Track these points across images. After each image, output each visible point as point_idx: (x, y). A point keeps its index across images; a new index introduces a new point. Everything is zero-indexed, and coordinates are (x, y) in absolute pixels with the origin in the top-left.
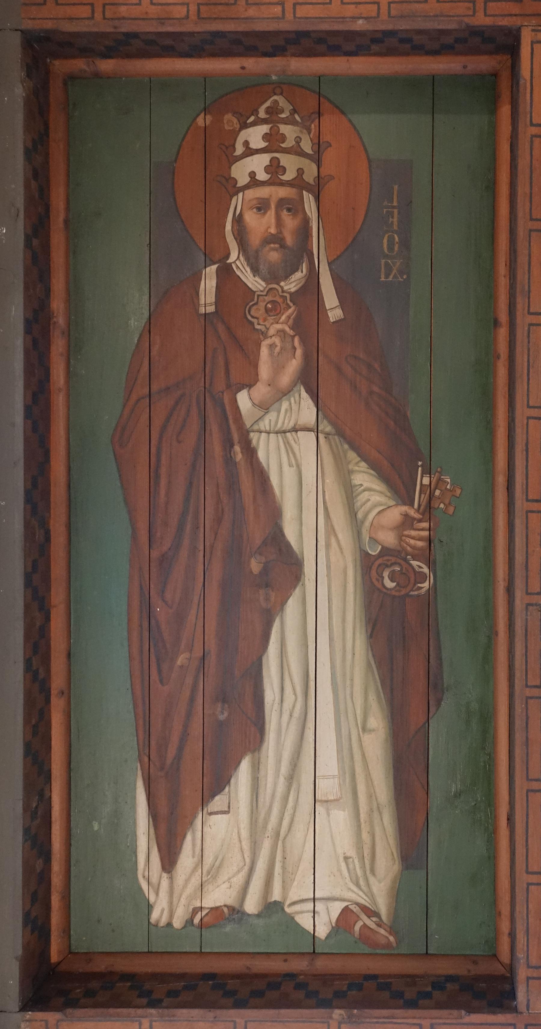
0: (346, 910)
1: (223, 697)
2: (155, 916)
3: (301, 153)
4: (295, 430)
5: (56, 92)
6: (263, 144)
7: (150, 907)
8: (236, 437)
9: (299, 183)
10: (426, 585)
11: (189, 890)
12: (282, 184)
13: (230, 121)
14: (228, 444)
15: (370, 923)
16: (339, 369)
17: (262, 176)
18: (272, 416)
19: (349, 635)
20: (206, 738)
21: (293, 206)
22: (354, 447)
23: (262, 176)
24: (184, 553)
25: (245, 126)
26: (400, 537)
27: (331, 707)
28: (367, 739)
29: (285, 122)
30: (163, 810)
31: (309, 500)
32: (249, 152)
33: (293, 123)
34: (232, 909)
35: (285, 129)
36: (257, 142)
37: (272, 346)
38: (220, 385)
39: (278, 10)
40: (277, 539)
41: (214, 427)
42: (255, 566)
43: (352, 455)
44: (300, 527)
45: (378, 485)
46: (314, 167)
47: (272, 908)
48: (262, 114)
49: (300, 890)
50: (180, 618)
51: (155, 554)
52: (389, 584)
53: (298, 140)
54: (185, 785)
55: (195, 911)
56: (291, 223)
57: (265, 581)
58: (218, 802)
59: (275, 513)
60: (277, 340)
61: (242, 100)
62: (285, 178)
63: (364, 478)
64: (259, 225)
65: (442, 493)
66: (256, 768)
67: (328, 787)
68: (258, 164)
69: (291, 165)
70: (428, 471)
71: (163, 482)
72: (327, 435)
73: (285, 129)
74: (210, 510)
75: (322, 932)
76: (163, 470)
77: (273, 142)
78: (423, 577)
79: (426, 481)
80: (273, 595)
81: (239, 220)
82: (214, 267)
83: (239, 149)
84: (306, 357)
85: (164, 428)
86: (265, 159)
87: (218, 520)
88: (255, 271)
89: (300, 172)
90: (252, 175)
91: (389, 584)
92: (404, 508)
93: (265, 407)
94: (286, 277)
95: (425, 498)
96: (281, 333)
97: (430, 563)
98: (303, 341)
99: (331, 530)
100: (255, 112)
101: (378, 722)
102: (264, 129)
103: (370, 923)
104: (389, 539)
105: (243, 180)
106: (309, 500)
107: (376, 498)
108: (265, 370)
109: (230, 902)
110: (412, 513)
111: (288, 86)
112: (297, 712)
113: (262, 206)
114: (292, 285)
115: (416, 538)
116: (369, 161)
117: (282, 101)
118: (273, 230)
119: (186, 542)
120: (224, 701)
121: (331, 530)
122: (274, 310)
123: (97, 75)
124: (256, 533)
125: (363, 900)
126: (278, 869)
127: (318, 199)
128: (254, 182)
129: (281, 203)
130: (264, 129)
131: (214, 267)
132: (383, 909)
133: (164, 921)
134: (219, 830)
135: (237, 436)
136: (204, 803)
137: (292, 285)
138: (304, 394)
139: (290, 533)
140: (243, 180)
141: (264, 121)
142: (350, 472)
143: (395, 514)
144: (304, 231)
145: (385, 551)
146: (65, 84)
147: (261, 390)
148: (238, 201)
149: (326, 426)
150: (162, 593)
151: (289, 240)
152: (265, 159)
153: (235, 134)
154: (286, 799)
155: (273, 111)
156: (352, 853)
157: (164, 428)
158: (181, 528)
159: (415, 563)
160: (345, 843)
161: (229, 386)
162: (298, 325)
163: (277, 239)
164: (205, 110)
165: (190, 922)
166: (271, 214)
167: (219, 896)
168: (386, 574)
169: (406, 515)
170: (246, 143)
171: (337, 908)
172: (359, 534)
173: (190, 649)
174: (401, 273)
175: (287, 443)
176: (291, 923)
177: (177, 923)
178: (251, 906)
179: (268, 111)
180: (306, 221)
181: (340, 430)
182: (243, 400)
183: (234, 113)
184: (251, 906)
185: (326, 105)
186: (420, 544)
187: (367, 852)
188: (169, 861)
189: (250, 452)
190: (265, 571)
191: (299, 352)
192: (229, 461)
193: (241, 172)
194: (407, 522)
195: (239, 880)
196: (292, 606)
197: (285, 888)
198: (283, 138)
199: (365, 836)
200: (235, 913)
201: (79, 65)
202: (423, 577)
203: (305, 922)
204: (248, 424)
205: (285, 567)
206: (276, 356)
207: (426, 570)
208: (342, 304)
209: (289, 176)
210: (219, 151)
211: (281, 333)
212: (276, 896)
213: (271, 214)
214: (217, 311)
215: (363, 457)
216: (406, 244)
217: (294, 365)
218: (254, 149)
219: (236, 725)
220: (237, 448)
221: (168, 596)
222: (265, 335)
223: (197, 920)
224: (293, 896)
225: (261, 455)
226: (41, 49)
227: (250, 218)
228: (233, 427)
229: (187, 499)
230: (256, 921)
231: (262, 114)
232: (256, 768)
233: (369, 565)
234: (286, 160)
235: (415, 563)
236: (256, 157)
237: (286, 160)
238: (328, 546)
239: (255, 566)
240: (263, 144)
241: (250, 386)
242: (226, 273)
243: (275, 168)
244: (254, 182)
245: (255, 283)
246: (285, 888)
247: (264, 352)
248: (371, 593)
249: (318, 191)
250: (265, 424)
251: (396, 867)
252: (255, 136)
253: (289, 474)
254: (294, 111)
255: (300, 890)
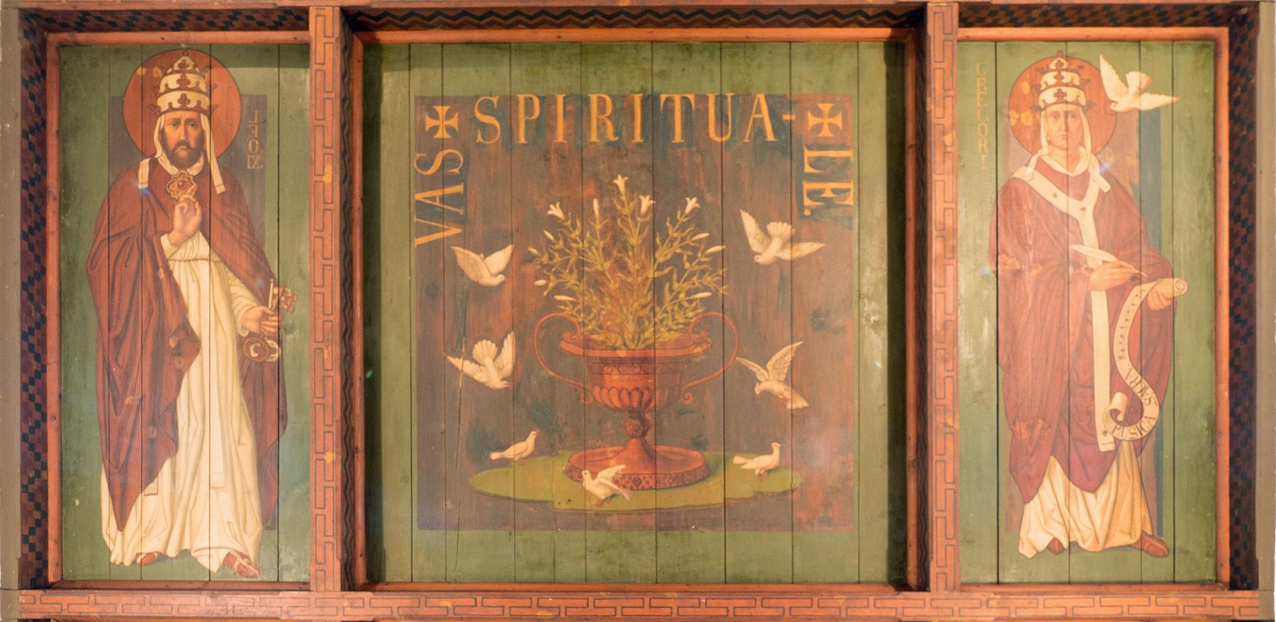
0: (229, 555)
1: (153, 422)
2: (113, 559)
3: (200, 92)
4: (195, 259)
5: (51, 53)
6: (177, 86)
7: (110, 553)
8: (160, 264)
9: (198, 109)
10: (276, 356)
11: (132, 544)
12: (188, 110)
13: (157, 71)
14: (156, 268)
15: (244, 562)
16: (222, 222)
17: (176, 105)
18: (182, 251)
19: (230, 386)
20: (145, 447)
21: (194, 123)
22: (231, 270)
23: (176, 105)
24: (130, 335)
25: (165, 74)
26: (260, 325)
27: (219, 425)
28: (240, 449)
29: (190, 72)
30: (118, 492)
31: (205, 303)
32: (168, 90)
33: (195, 73)
34: (160, 554)
35: (189, 76)
36: (174, 85)
37: (182, 209)
38: (150, 232)
39: (597, 603)
40: (185, 327)
41: (147, 258)
42: (172, 343)
43: (231, 275)
44: (199, 319)
45: (247, 294)
46: (207, 99)
47: (184, 553)
48: (176, 67)
49: (202, 542)
50: (127, 374)
51: (112, 335)
52: (254, 355)
53: (198, 83)
54: (134, 471)
55: (137, 555)
56: (193, 133)
57: (178, 352)
58: (151, 488)
59: (184, 310)
60: (185, 205)
61: (164, 57)
62: (190, 106)
63: (238, 289)
64: (175, 135)
65: (287, 298)
66: (174, 466)
67: (219, 478)
68: (173, 98)
69: (193, 98)
70: (278, 285)
71: (117, 291)
72: (216, 263)
73: (189, 76)
74: (145, 309)
75: (214, 569)
76: (117, 284)
77: (183, 84)
78: (274, 351)
79: (276, 291)
80: (183, 360)
81: (162, 132)
82: (147, 160)
83: (162, 89)
84: (203, 215)
85: (117, 258)
86: (178, 95)
87: (150, 314)
88: (173, 163)
89: (199, 102)
90: (170, 104)
91: (254, 355)
92: (263, 308)
93: (178, 245)
94: (190, 166)
95: (276, 302)
96: (188, 200)
97: (279, 342)
98: (201, 205)
99: (218, 321)
100: (172, 66)
101: (248, 440)
102: (178, 76)
103: (244, 562)
104: (253, 327)
105: (164, 107)
106: (205, 303)
107: (246, 301)
108: (178, 222)
109: (159, 549)
110: (267, 311)
111: (192, 49)
112: (199, 433)
113: (176, 123)
114: (195, 170)
115: (271, 325)
116: (241, 96)
117: (188, 60)
118: (183, 138)
119: (131, 329)
120: (154, 425)
121: (218, 321)
122: (183, 186)
123: (77, 44)
124: (173, 322)
125: (240, 549)
126: (187, 527)
127: (210, 119)
128: (171, 109)
129: (188, 121)
130: (178, 76)
131: (147, 160)
132: (252, 555)
133: (118, 562)
134: (151, 506)
135: (160, 263)
136: (142, 489)
137: (195, 170)
138: (202, 237)
139: (193, 323)
140: (164, 107)
141: (177, 72)
142: (230, 285)
143: (258, 311)
144: (201, 139)
145: (251, 335)
146: (58, 50)
147: (175, 235)
148: (161, 121)
149: (215, 258)
150: (116, 360)
151: (192, 144)
152: (178, 95)
153: (159, 80)
154: (191, 486)
155: (182, 66)
156: (232, 519)
157: (117, 258)
158: (128, 317)
159: (269, 342)
160: (228, 514)
161: (156, 233)
162: (198, 195)
163: (185, 143)
164: (142, 65)
165: (134, 562)
166: (182, 127)
167: (153, 546)
168: (252, 348)
169: (264, 313)
170: (167, 85)
171: (223, 553)
172: (235, 323)
173: (134, 393)
174: (260, 163)
175: (192, 270)
176: (195, 563)
177: (127, 563)
178: (172, 552)
179: (180, 66)
180: (203, 132)
181: (224, 259)
182: (165, 241)
183: (160, 67)
184: (172, 552)
185: (214, 62)
186: (273, 330)
187: (241, 518)
188: (121, 525)
189: (169, 273)
190: (178, 346)
191: (199, 212)
192: (156, 279)
193: (163, 103)
194: (265, 316)
195: (164, 536)
196: (195, 367)
197: (192, 541)
198: (189, 82)
199: (241, 510)
200: (162, 557)
201: (65, 36)
202: (274, 351)
203: (204, 561)
204: (168, 255)
205: (190, 344)
206: (186, 215)
207: (276, 346)
208: (225, 183)
209: (192, 105)
210: (150, 90)
211: (188, 200)
212: (186, 546)
213: (182, 127)
214: (149, 188)
215: (238, 277)
216: (262, 146)
217: (195, 219)
218: (469, 279)
219: (160, 438)
220: (161, 270)
221: (120, 362)
222: (178, 201)
223: (138, 561)
224: (197, 545)
225: (176, 275)
226: (38, 24)
227: (169, 131)
228: (159, 258)
229: (132, 300)
230: (175, 561)
231: (176, 67)
232: (174, 466)
233: (242, 343)
234: (190, 95)
235: (269, 342)
236: (172, 94)
237: (190, 95)
238: (216, 330)
239: (172, 343)
240: (177, 86)
241: (169, 233)
242: (154, 164)
243: (184, 100)
244: (171, 109)
245: (172, 170)
246: (192, 541)
247: (177, 211)
248: (243, 359)
249: (210, 113)
250: (178, 255)
251: (260, 528)
252: (172, 80)
253: (193, 287)
254: (195, 66)
255: (202, 542)
